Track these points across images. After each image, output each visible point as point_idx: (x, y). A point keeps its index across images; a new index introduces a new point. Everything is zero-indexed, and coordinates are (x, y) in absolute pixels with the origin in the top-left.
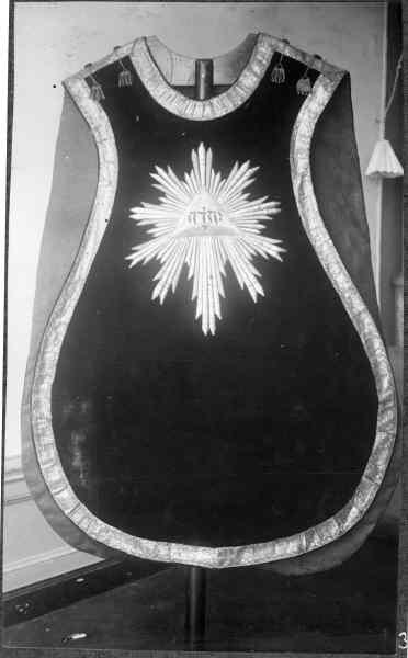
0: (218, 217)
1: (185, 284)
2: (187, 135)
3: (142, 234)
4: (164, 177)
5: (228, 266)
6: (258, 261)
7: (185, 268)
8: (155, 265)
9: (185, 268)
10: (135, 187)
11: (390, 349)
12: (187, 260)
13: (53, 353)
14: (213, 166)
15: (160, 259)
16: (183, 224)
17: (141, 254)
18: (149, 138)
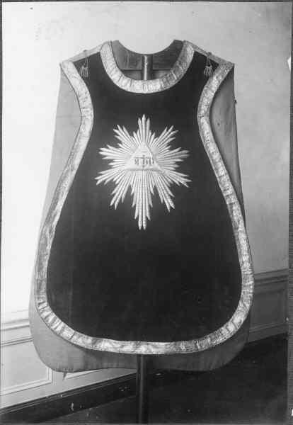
0: (152, 161)
1: (129, 197)
2: (191, 412)
3: (106, 164)
4: (121, 133)
5: (155, 189)
6: (173, 187)
7: (130, 189)
8: (112, 185)
9: (130, 189)
10: (103, 135)
11: (178, 47)
12: (131, 183)
13: (46, 264)
14: (151, 129)
15: (115, 181)
16: (131, 164)
17: (104, 177)
18: (114, 110)
